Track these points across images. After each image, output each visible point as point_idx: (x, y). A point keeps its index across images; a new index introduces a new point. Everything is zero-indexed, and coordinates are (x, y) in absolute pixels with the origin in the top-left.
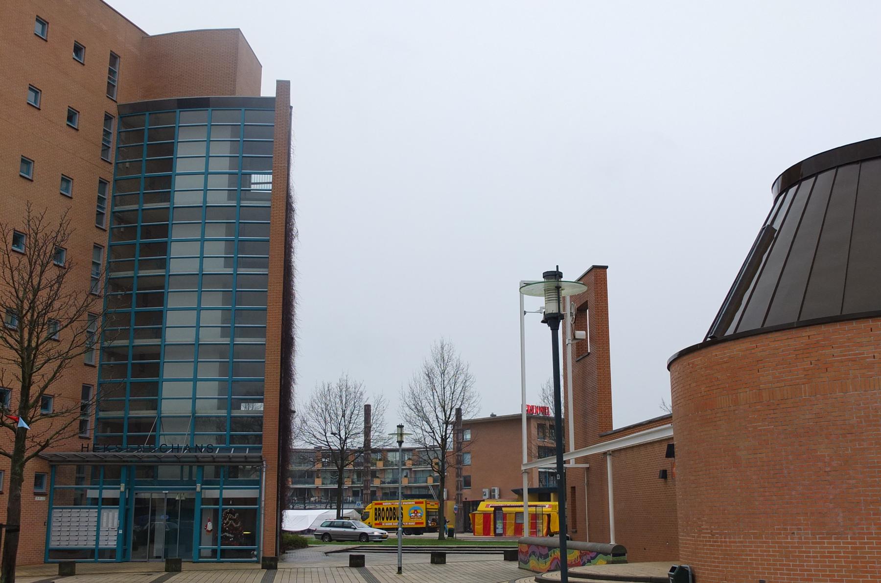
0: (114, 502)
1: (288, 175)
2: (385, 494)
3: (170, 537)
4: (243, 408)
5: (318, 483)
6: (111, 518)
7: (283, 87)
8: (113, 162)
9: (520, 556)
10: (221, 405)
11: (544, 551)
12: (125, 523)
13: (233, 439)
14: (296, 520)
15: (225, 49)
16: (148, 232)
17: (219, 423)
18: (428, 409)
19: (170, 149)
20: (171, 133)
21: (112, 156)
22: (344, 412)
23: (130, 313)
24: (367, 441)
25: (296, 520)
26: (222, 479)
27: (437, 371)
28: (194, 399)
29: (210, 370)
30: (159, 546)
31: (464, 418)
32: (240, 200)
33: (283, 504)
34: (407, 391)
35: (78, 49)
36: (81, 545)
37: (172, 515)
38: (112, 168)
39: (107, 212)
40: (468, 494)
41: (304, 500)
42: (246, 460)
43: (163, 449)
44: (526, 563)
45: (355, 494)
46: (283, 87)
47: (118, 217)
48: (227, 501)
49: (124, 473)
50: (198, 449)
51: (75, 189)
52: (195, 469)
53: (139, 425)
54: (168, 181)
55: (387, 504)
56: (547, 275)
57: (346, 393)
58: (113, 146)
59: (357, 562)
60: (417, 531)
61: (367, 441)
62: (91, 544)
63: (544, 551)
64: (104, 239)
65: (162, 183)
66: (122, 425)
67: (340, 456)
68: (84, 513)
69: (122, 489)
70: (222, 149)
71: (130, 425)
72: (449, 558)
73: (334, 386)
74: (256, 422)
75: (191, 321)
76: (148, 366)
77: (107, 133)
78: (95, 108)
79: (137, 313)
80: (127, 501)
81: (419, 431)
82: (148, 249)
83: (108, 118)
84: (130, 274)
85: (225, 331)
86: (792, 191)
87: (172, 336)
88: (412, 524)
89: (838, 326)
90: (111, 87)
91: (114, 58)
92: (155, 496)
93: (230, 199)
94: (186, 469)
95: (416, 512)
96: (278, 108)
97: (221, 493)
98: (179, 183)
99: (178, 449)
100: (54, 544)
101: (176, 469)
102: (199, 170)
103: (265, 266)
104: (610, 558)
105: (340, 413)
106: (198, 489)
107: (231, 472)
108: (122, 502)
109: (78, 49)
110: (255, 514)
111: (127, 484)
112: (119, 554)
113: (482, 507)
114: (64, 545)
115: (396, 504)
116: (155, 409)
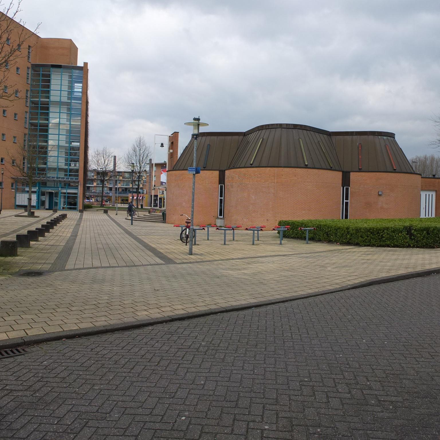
7: (86, 64)
8: (30, 84)
10: (66, 164)
11: (155, 210)
13: (70, 175)
17: (65, 170)
19: (49, 81)
20: (49, 76)
23: (38, 112)
27: (138, 149)
32: (71, 100)
34: (126, 156)
38: (29, 86)
39: (29, 100)
46: (86, 64)
48: (68, 193)
49: (38, 184)
52: (58, 183)
53: (42, 147)
64: (28, 110)
66: (38, 125)
67: (104, 173)
69: (37, 189)
70: (66, 83)
71: (39, 147)
74: (78, 149)
79: (40, 112)
80: (39, 192)
94: (56, 184)
97: (67, 191)
99: (54, 177)
100: (17, 204)
102: (58, 84)
106: (60, 189)
107: (68, 185)
108: (37, 192)
110: (76, 197)
111: (39, 187)
112: (37, 207)
114: (20, 204)
116: (49, 99)
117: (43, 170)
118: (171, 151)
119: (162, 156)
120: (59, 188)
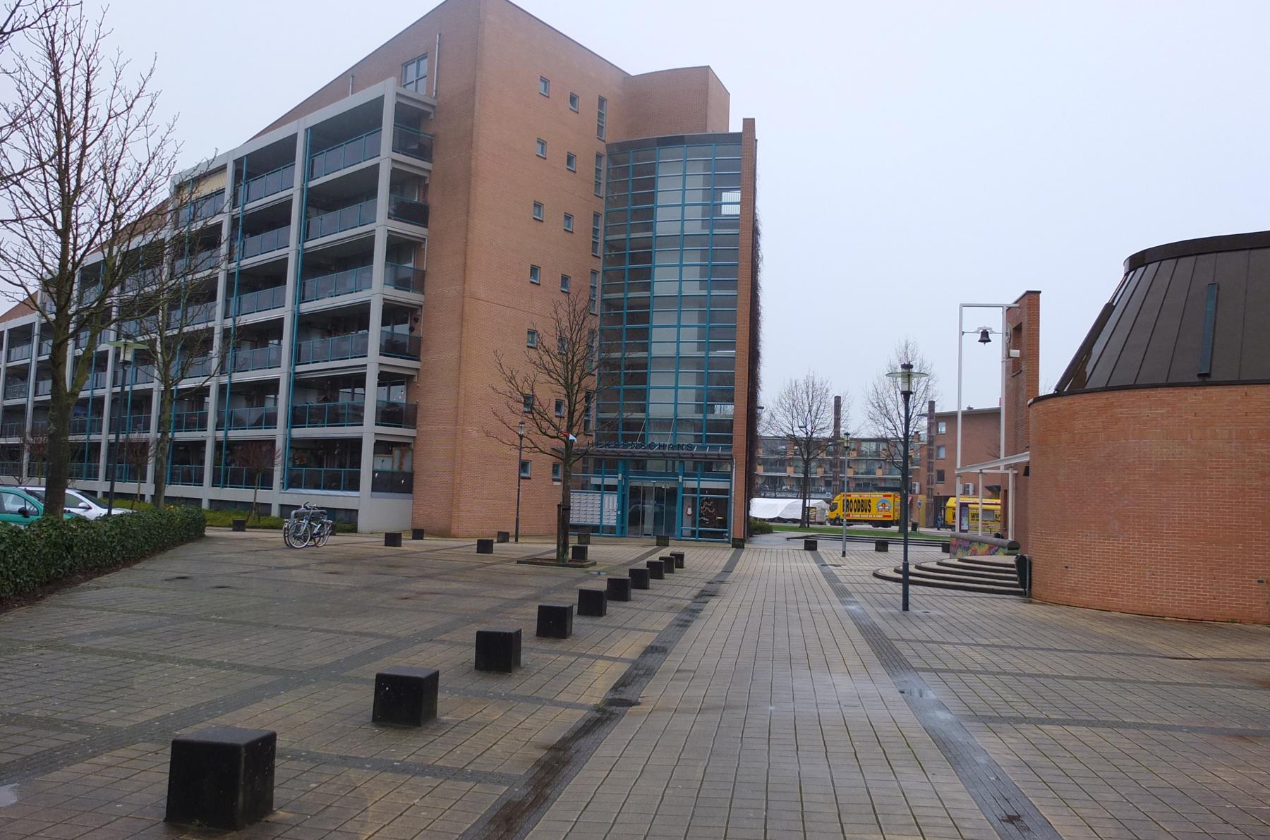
0: (611, 488)
1: (754, 214)
2: (858, 485)
3: (658, 518)
4: (717, 412)
5: (790, 471)
6: (612, 501)
7: (749, 124)
9: (952, 549)
10: (699, 409)
11: (967, 544)
12: (622, 506)
13: (709, 439)
14: (763, 508)
15: (698, 87)
16: (634, 258)
18: (891, 406)
19: (652, 183)
20: (652, 169)
21: (603, 192)
22: (810, 407)
24: (837, 432)
25: (763, 508)
26: (699, 472)
28: (676, 404)
29: (689, 380)
30: (649, 526)
31: (937, 410)
33: (751, 491)
34: (871, 388)
35: (573, 99)
36: (589, 522)
37: (659, 499)
39: (601, 241)
40: (940, 489)
41: (774, 488)
42: (719, 457)
43: (651, 446)
44: (955, 554)
45: (828, 484)
46: (749, 124)
47: (610, 245)
48: (703, 491)
49: (620, 465)
50: (679, 447)
51: (575, 225)
52: (677, 463)
54: (650, 213)
55: (855, 496)
56: (904, 366)
57: (813, 390)
58: (603, 182)
59: (811, 546)
60: (886, 524)
61: (837, 432)
62: (596, 522)
63: (967, 544)
64: (599, 265)
65: (647, 216)
67: (808, 446)
68: (590, 496)
70: (696, 183)
72: (890, 547)
73: (801, 382)
74: (727, 425)
75: (671, 338)
76: (638, 375)
77: (598, 171)
78: (588, 148)
81: (881, 428)
82: (635, 274)
83: (599, 156)
84: (621, 295)
85: (701, 347)
86: (1141, 270)
87: (657, 350)
88: (880, 517)
89: (1126, 392)
90: (600, 128)
91: (602, 101)
92: (647, 484)
93: (703, 228)
94: (670, 463)
95: (884, 505)
96: (745, 141)
98: (661, 214)
99: (664, 446)
101: (662, 463)
102: (677, 202)
103: (735, 288)
104: (1006, 551)
105: (807, 409)
107: (706, 467)
108: (620, 488)
109: (573, 99)
112: (618, 531)
113: (951, 502)
115: (866, 496)
117: (638, 425)
118: (1015, 353)
119: (980, 383)
120: (676, 475)
